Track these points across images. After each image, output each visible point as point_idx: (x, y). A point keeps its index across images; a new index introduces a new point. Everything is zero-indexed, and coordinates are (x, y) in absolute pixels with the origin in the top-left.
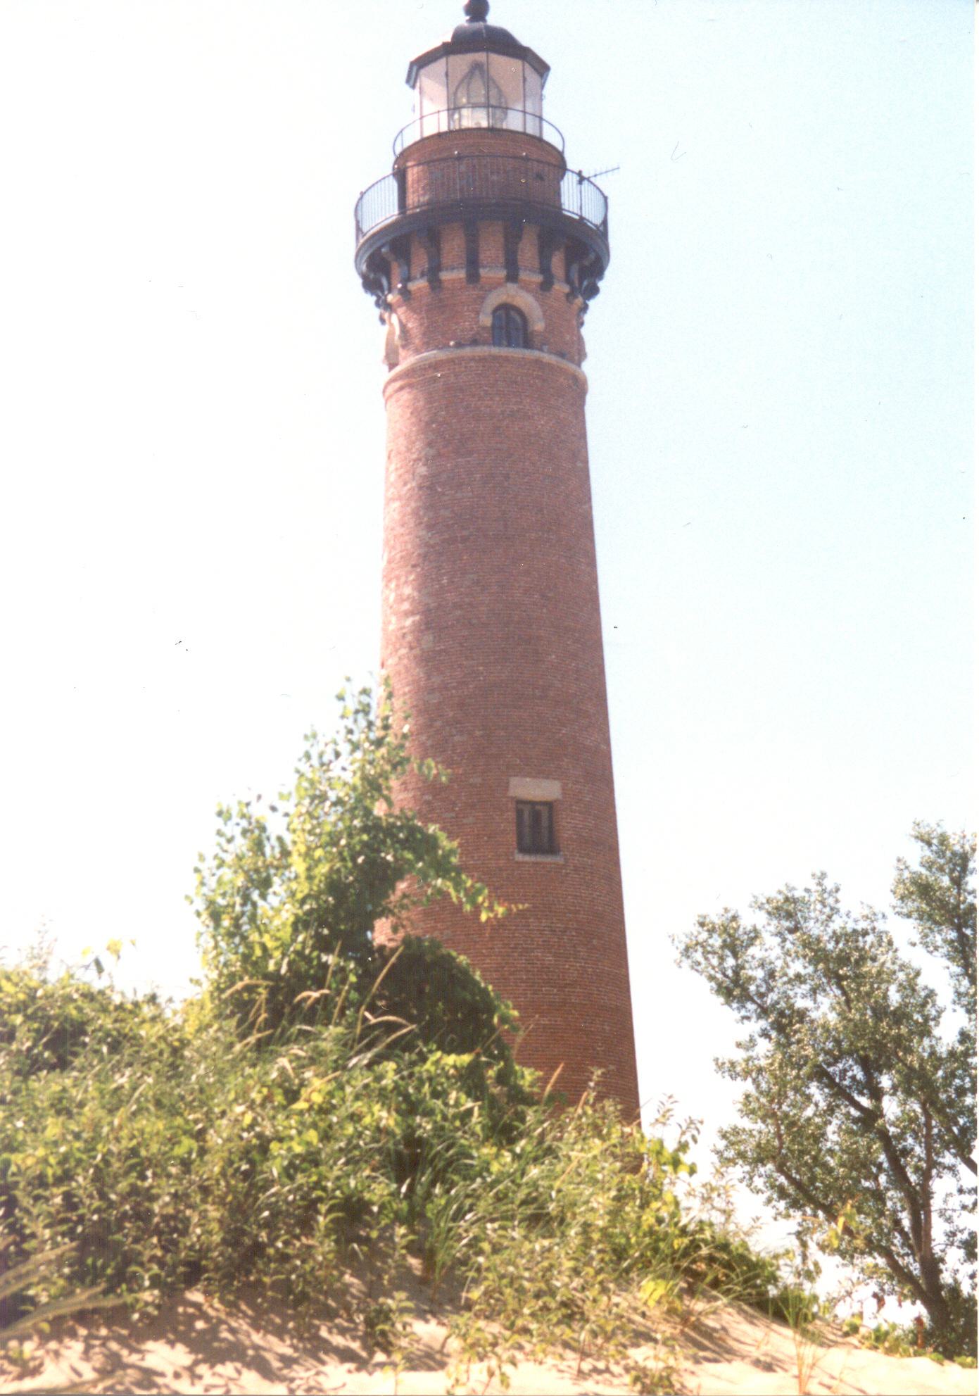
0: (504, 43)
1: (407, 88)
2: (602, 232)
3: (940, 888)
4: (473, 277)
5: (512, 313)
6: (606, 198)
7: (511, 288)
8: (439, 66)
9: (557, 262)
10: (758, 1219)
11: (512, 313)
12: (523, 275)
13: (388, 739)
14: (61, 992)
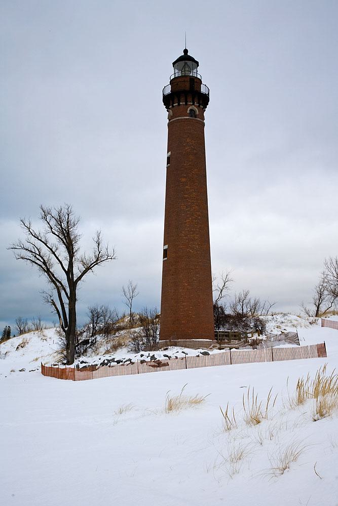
4: (186, 104)
12: (195, 104)
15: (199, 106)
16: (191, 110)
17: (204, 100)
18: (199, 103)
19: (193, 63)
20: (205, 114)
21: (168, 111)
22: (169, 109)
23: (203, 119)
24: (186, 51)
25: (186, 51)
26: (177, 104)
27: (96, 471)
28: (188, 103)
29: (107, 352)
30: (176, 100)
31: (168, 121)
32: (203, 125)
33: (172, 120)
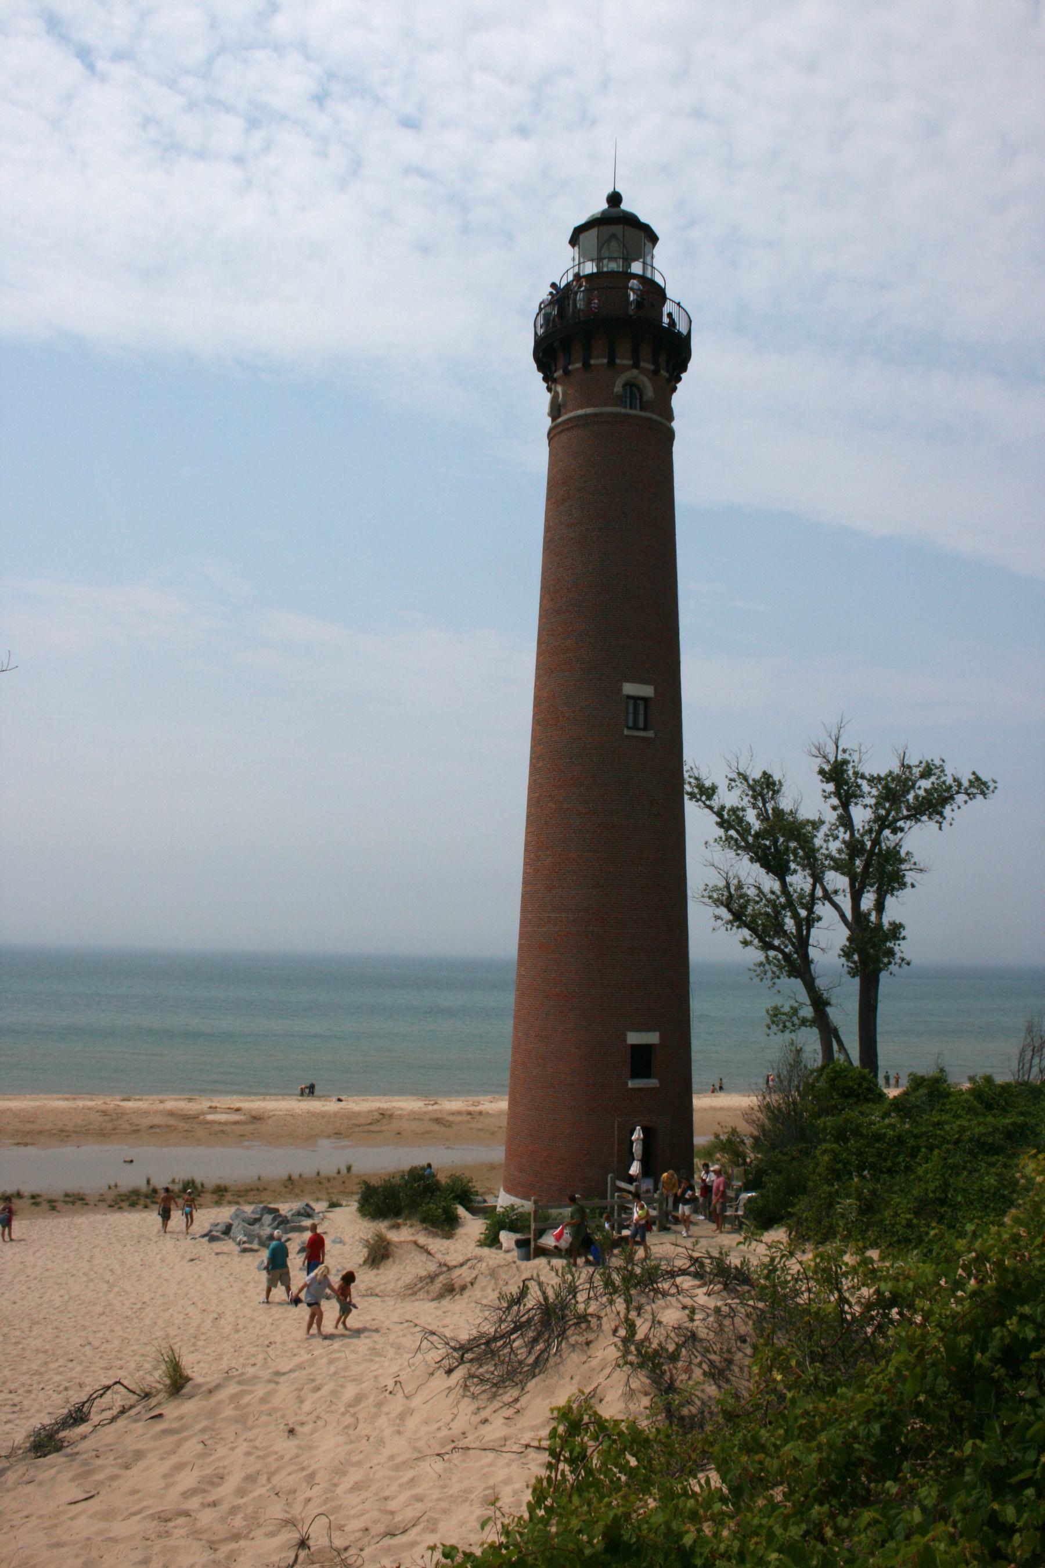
0: (631, 221)
1: (570, 247)
2: (688, 338)
3: (909, 1295)
4: (611, 363)
5: (634, 389)
6: (691, 322)
7: (635, 372)
8: (593, 233)
9: (662, 361)
10: (706, 843)
11: (634, 389)
12: (643, 364)
13: (947, 1127)
14: (400, 1221)
15: (656, 372)
16: (630, 385)
17: (673, 352)
18: (655, 362)
19: (629, 230)
20: (679, 400)
21: (549, 389)
22: (555, 381)
23: (670, 417)
24: (615, 199)
25: (615, 199)
26: (579, 365)
27: (217, 1254)
28: (618, 361)
29: (480, 1260)
30: (561, 363)
31: (548, 422)
32: (669, 436)
33: (560, 420)
